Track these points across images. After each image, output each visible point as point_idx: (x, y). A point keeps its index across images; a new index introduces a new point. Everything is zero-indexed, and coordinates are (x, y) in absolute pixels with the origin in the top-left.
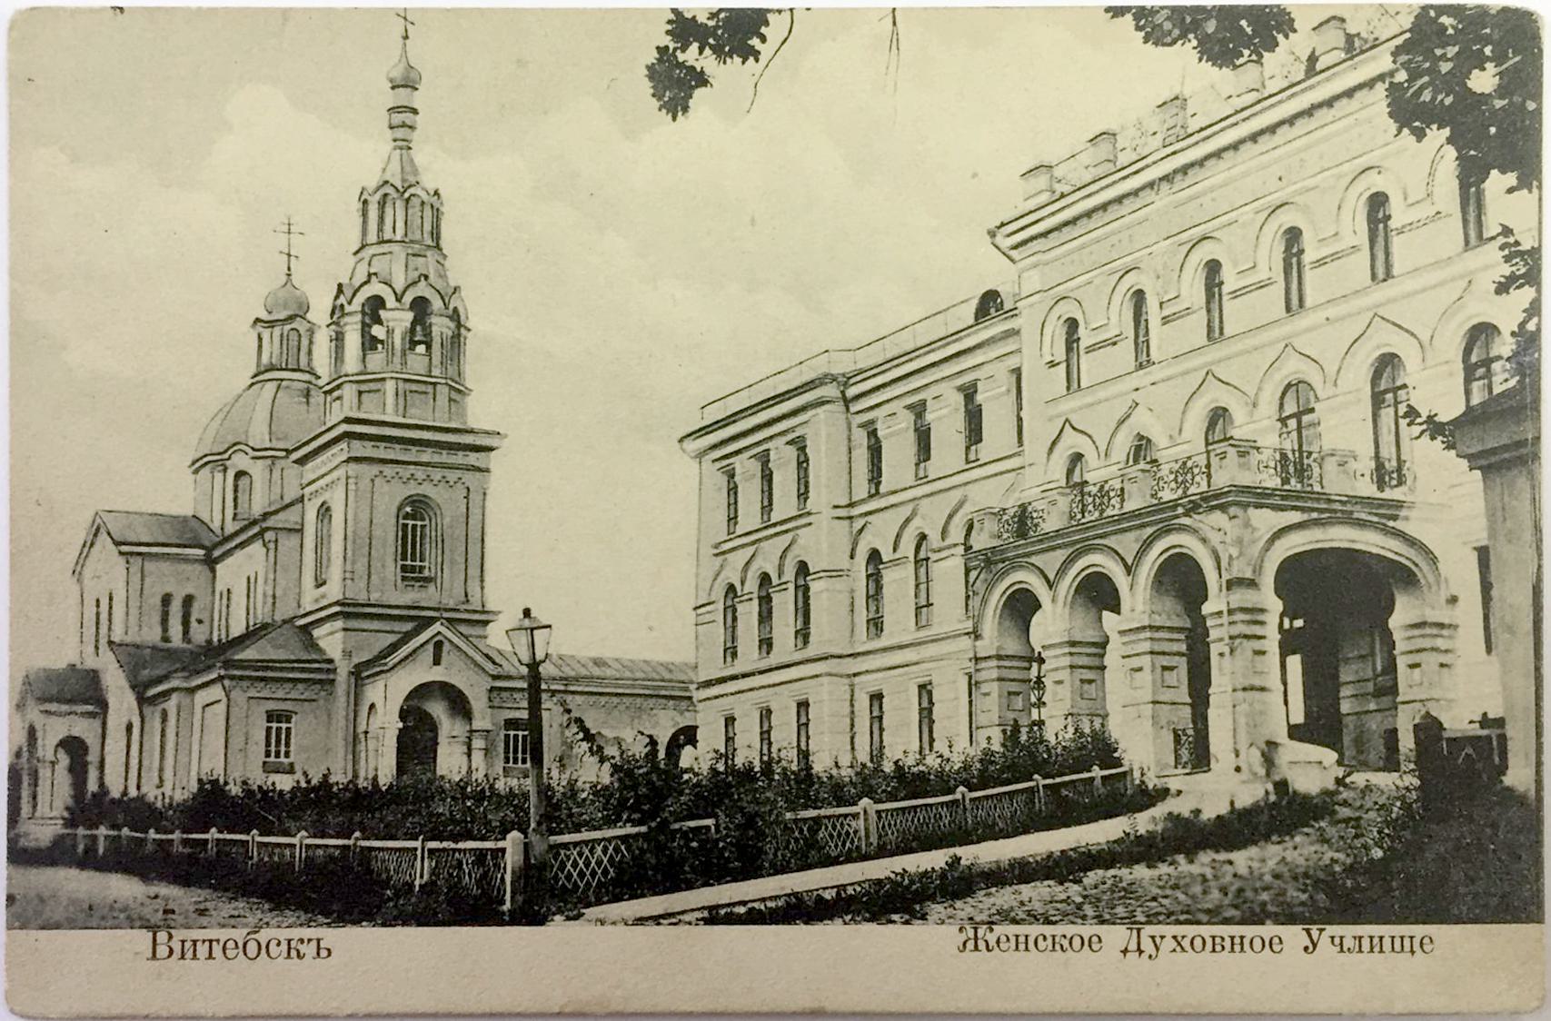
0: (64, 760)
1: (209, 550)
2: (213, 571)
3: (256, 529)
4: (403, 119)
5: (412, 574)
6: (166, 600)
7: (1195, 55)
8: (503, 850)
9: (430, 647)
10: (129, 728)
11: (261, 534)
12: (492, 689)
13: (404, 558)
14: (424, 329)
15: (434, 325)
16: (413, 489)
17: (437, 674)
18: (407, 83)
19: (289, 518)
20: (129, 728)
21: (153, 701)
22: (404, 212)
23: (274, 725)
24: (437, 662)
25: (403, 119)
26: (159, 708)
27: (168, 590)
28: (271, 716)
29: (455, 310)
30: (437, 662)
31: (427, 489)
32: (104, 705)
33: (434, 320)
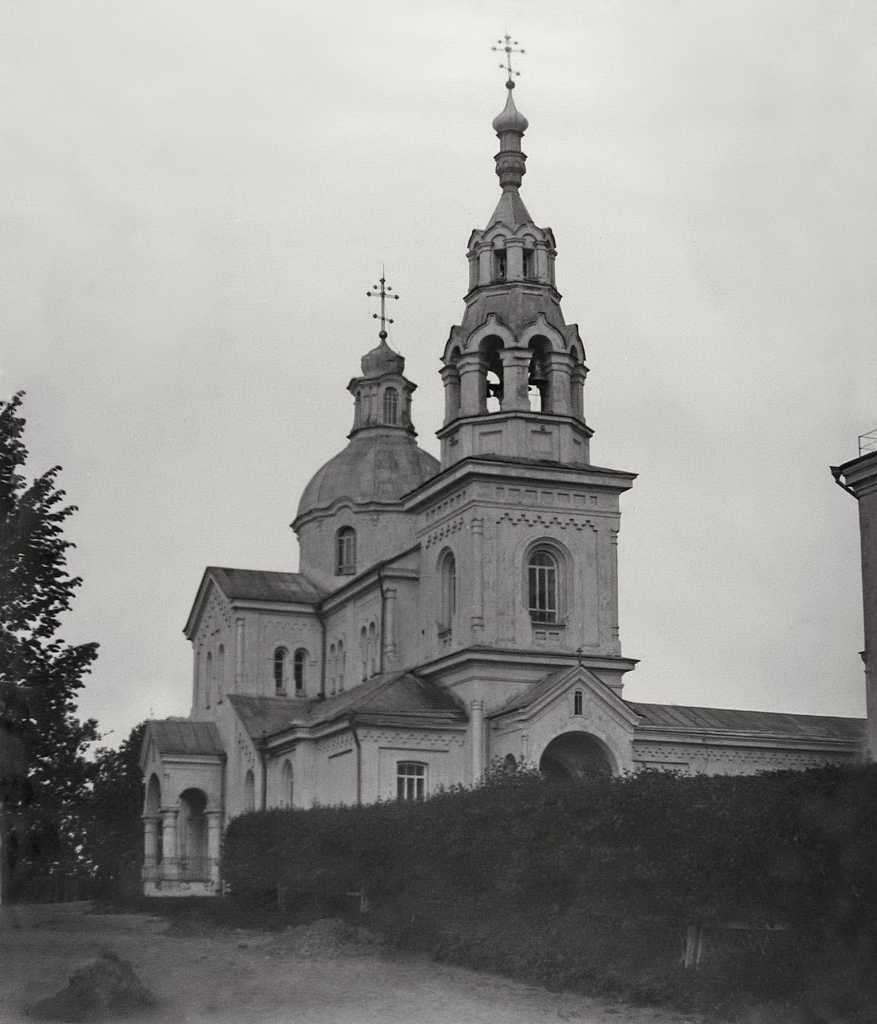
0: (185, 813)
1: (319, 606)
2: (324, 626)
3: (374, 578)
4: (511, 169)
5: (543, 617)
6: (279, 654)
7: (79, 598)
8: (553, 571)
9: (572, 698)
10: (250, 775)
11: (381, 580)
12: (636, 741)
13: (532, 604)
14: (543, 368)
15: (553, 359)
16: (539, 532)
17: (575, 725)
18: (510, 85)
19: (409, 564)
20: (250, 775)
21: (275, 753)
22: (513, 264)
23: (406, 777)
24: (578, 710)
25: (511, 169)
26: (282, 760)
27: (278, 644)
28: (402, 767)
29: (573, 348)
30: (578, 710)
31: (555, 532)
32: (223, 757)
33: (554, 359)
